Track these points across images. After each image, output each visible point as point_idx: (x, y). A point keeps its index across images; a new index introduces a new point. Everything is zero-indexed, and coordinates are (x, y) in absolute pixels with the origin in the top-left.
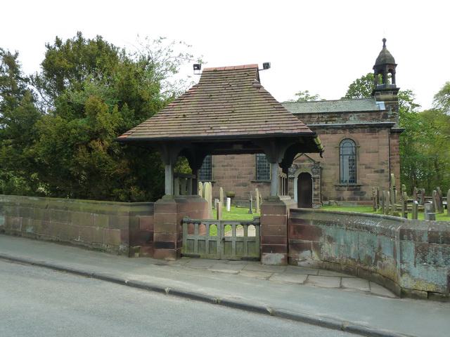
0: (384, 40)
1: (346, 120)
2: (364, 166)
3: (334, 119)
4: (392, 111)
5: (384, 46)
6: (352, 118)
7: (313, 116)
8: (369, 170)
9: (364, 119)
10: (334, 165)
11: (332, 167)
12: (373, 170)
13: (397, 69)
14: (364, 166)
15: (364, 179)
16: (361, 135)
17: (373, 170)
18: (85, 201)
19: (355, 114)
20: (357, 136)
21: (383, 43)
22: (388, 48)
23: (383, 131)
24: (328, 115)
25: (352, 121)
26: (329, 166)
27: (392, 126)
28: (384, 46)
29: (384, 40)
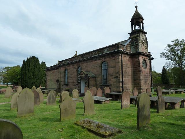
0: (136, 7)
1: (103, 52)
2: (110, 75)
3: (99, 53)
4: (135, 43)
5: (136, 10)
6: (105, 51)
7: (93, 53)
8: (112, 77)
9: (110, 50)
10: (99, 75)
11: (99, 76)
12: (114, 77)
13: (144, 21)
14: (110, 75)
15: (110, 82)
16: (108, 59)
17: (114, 77)
18: (183, 115)
19: (106, 49)
20: (107, 59)
21: (135, 9)
22: (139, 11)
23: (117, 55)
24: (97, 52)
25: (106, 52)
26: (98, 76)
27: (150, 56)
28: (136, 10)
29: (136, 7)
